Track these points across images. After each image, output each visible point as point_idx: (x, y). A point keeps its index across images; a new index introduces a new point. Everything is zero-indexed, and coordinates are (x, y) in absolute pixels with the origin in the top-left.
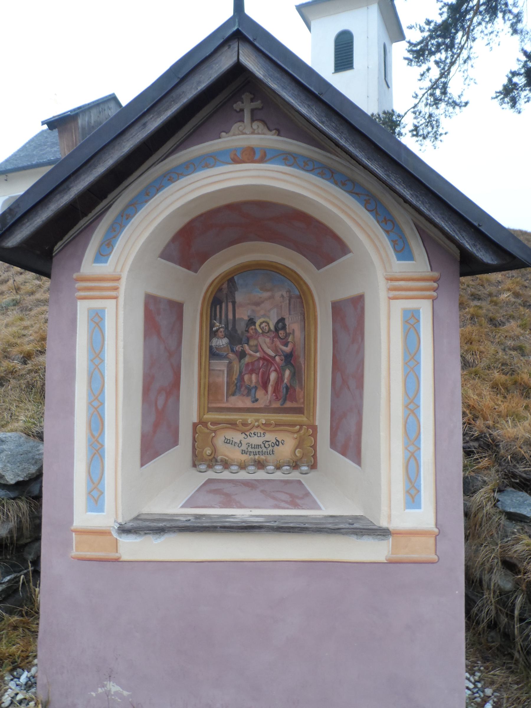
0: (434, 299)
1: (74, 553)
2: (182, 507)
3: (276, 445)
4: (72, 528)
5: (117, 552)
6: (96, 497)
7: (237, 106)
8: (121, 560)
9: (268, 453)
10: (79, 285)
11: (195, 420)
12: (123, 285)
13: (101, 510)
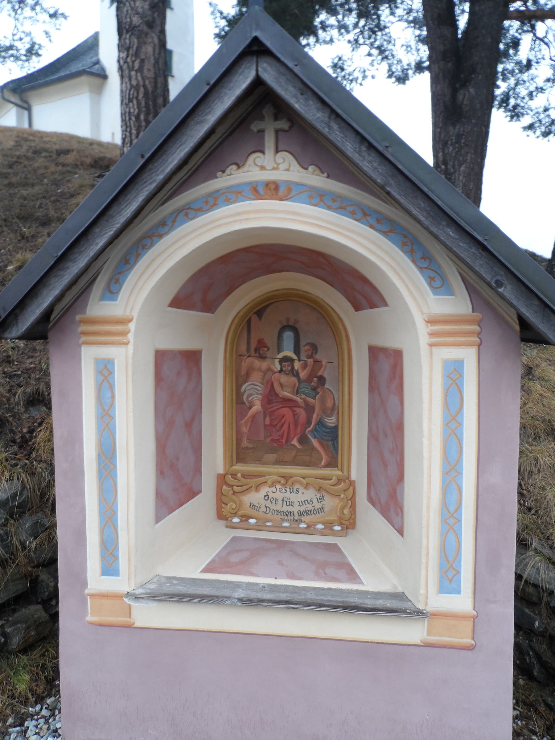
1: (89, 618)
5: (130, 617)
6: (450, 577)
7: (255, 127)
8: (135, 626)
11: (221, 471)
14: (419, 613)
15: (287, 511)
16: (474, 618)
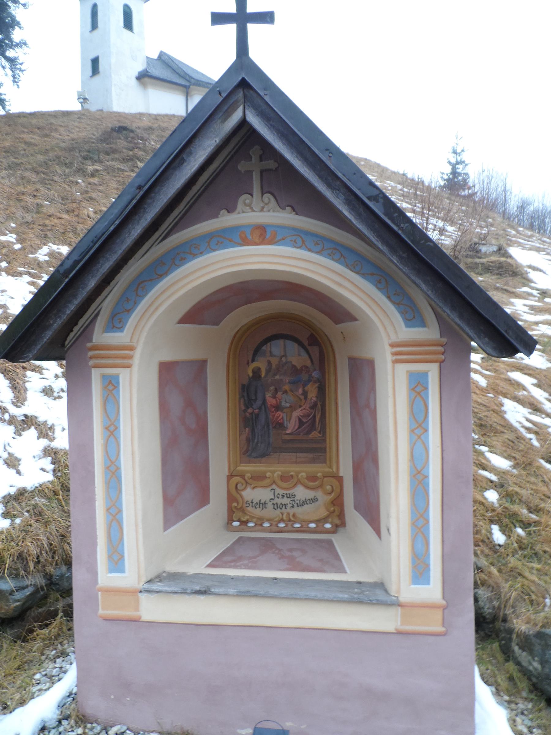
0: (441, 362)
1: (101, 612)
3: (280, 508)
4: (98, 586)
7: (243, 166)
8: (141, 620)
9: (299, 504)
10: (91, 353)
12: (137, 354)
13: (122, 571)
14: (397, 604)
15: (281, 504)
16: (445, 608)
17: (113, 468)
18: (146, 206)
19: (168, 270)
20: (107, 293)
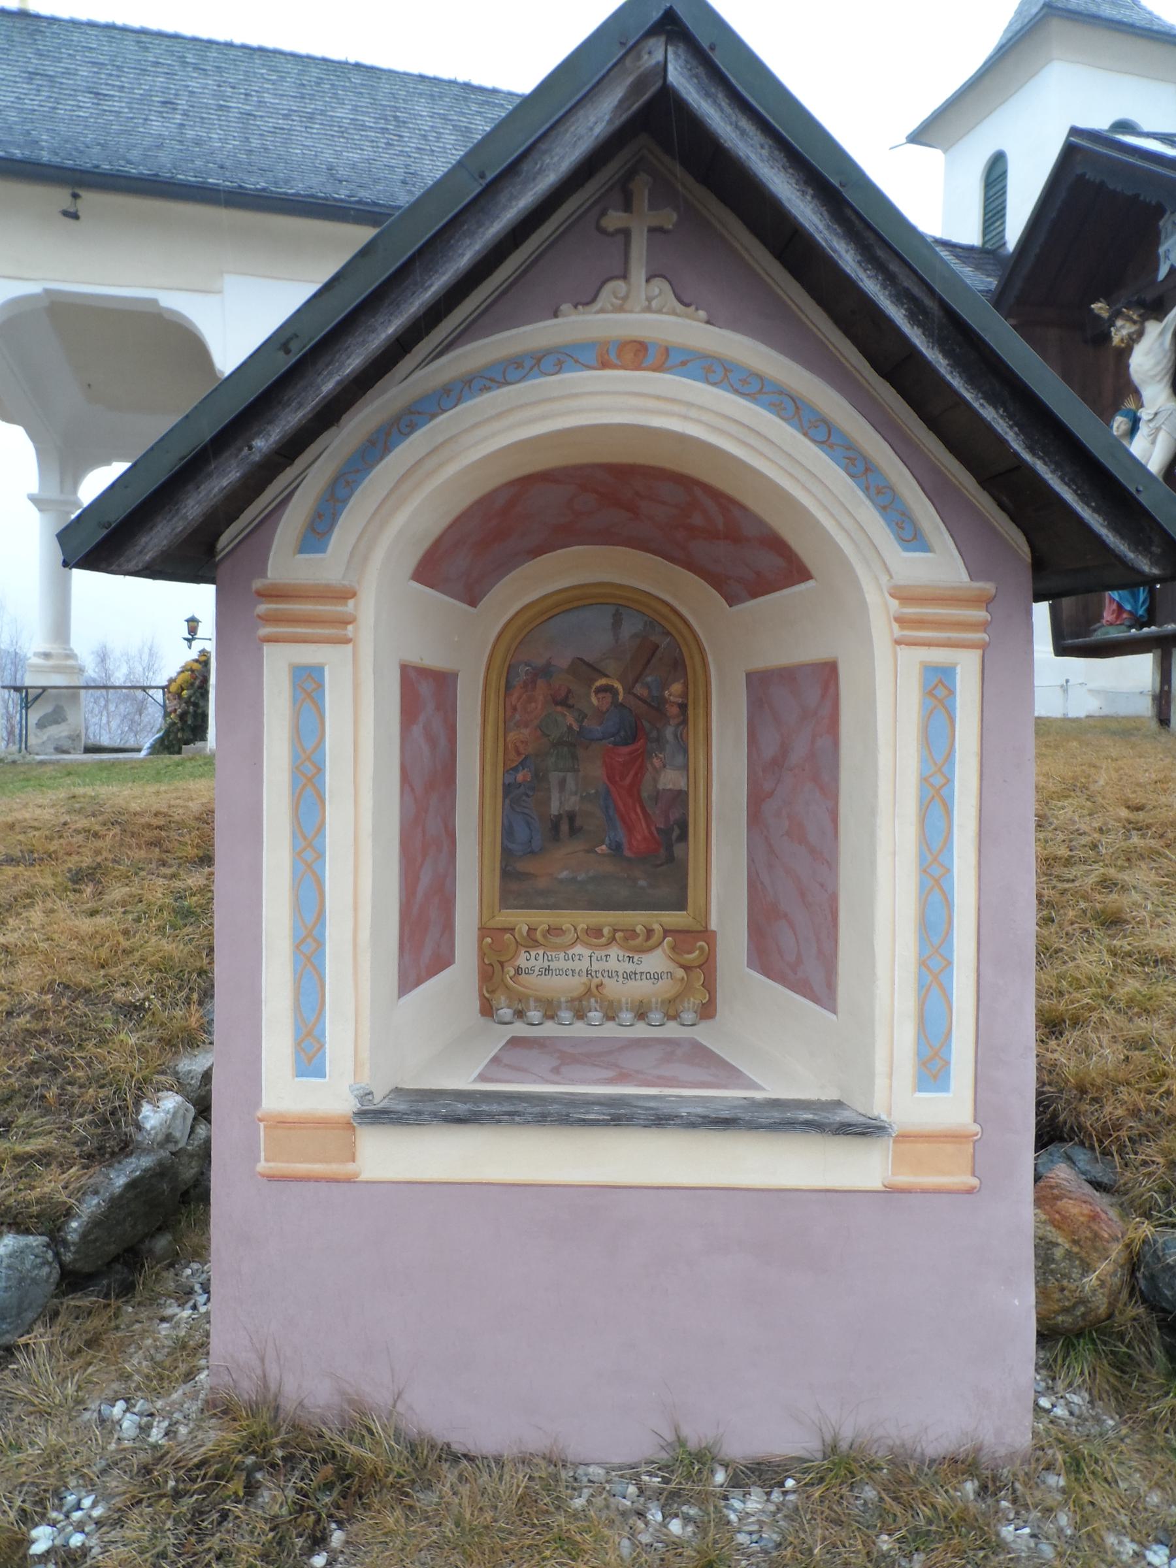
0: (984, 647)
1: (262, 1166)
2: (475, 1081)
4: (259, 1114)
17: (309, 855)
18: (245, 1384)
19: (125, 177)
20: (312, 459)
